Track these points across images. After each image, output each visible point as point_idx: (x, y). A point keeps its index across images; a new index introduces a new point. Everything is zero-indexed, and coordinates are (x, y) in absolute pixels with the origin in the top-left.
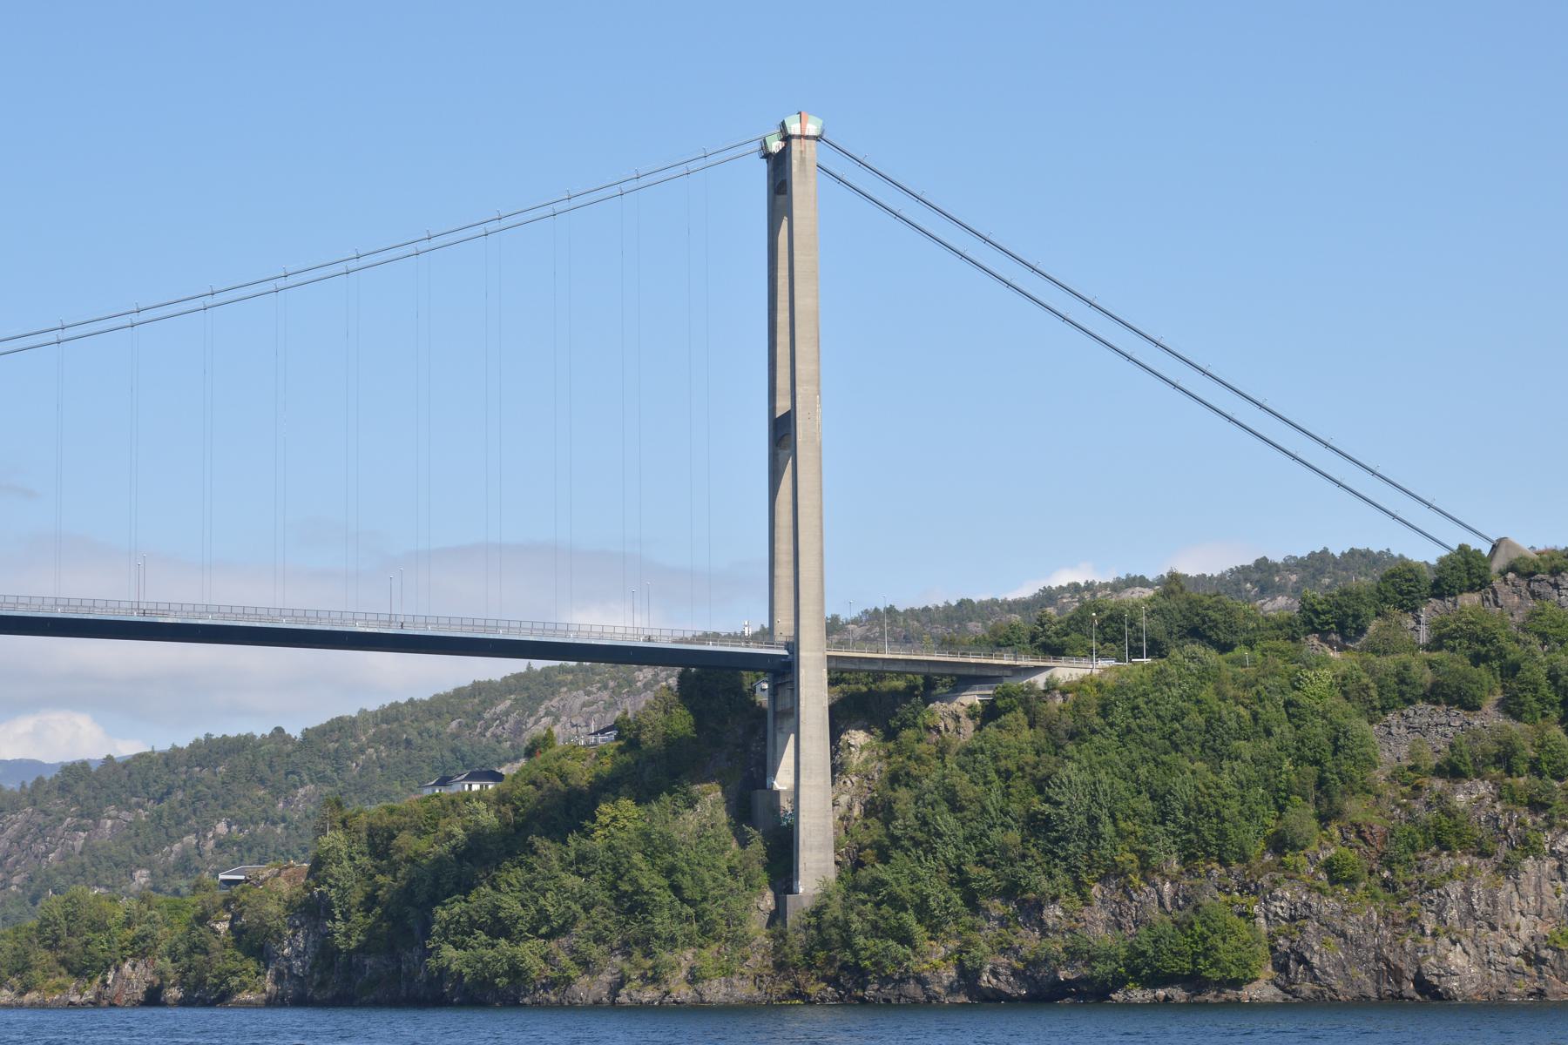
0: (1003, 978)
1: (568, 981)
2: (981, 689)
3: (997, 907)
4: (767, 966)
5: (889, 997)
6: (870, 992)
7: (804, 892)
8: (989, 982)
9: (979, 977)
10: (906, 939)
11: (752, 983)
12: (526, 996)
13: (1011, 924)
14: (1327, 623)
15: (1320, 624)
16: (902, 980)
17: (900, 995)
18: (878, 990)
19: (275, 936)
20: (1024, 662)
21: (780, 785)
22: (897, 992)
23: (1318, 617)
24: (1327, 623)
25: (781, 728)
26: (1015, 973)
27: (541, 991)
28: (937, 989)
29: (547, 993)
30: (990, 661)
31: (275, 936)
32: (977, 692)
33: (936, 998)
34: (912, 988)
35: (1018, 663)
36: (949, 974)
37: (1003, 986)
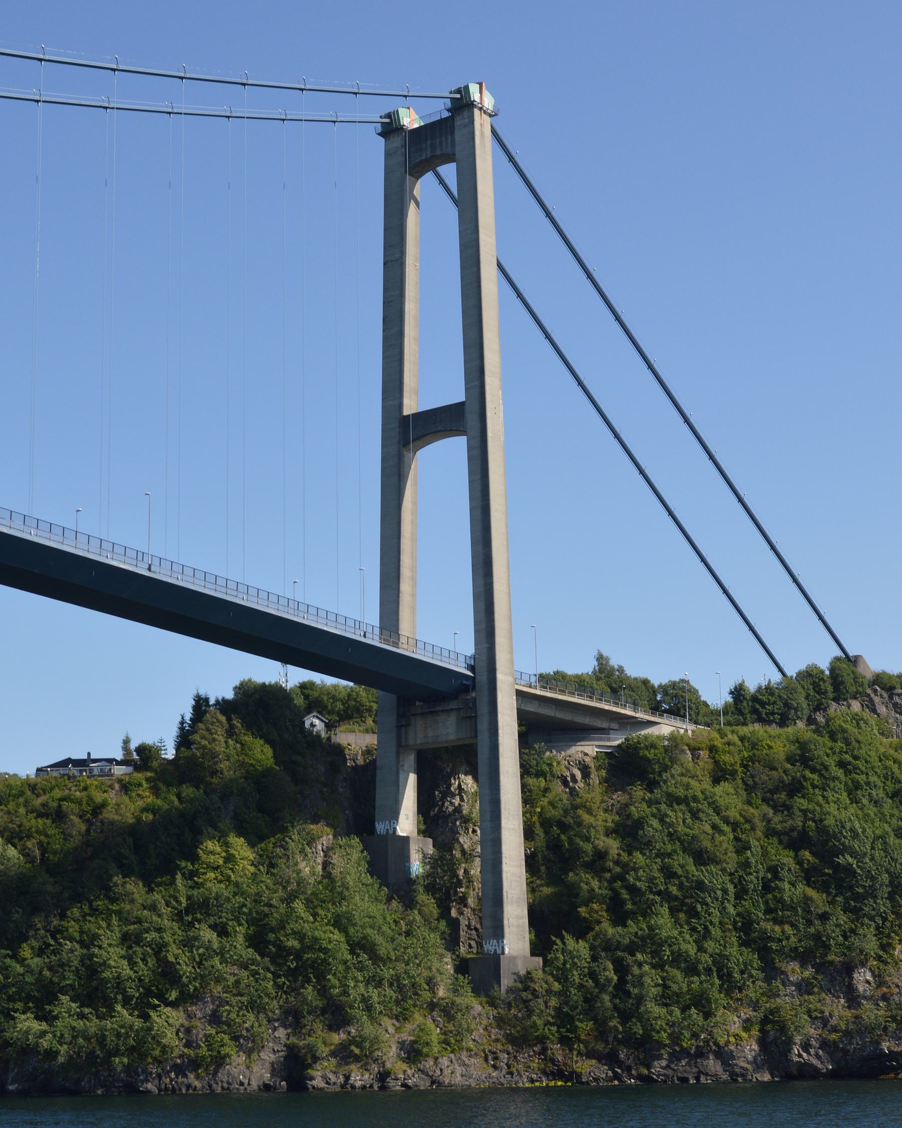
0: (812, 1051)
1: (220, 1061)
2: (600, 740)
3: (795, 971)
4: (497, 1040)
5: (686, 1075)
6: (658, 1067)
7: (509, 953)
8: (800, 1056)
9: (790, 1050)
10: (701, 1002)
11: (481, 1061)
12: (147, 1081)
13: (816, 990)
14: (773, 714)
15: (766, 714)
16: (701, 1054)
17: (700, 1072)
18: (668, 1067)
19: (585, 1027)
20: (641, 715)
21: (402, 831)
22: (695, 1070)
23: (763, 707)
24: (773, 714)
25: (403, 766)
26: (824, 1044)
27: (173, 1075)
28: (742, 1064)
29: (186, 1076)
30: (615, 709)
31: (585, 1027)
32: (597, 743)
33: (743, 1075)
34: (712, 1064)
35: (637, 715)
36: (750, 1049)
37: (815, 1062)
